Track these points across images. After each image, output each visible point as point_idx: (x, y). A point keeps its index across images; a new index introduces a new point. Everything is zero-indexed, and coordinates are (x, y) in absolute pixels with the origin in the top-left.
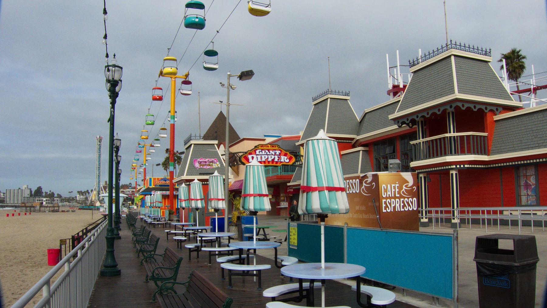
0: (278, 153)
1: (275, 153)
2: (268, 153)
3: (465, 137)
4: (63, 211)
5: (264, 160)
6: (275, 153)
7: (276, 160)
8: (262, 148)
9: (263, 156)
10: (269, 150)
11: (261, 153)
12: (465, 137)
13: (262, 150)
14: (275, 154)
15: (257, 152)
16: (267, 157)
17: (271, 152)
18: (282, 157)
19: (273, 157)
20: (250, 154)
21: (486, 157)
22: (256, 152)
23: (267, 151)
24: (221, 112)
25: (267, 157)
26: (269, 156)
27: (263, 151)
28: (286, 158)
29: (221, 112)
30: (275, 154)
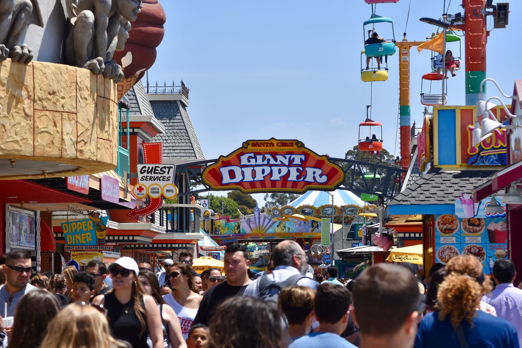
0: (297, 161)
1: (291, 162)
2: (272, 162)
3: (184, 210)
4: (333, 201)
5: (259, 177)
6: (291, 162)
7: (293, 177)
8: (257, 149)
9: (259, 170)
10: (274, 155)
11: (253, 162)
12: (184, 210)
13: (256, 154)
14: (291, 163)
15: (244, 160)
16: (267, 170)
17: (280, 158)
18: (310, 171)
19: (284, 170)
20: (226, 164)
21: (116, 224)
22: (240, 160)
23: (268, 156)
24: (150, 101)
25: (267, 170)
26: (275, 169)
27: (260, 158)
28: (319, 172)
29: (150, 101)
30: (291, 163)
